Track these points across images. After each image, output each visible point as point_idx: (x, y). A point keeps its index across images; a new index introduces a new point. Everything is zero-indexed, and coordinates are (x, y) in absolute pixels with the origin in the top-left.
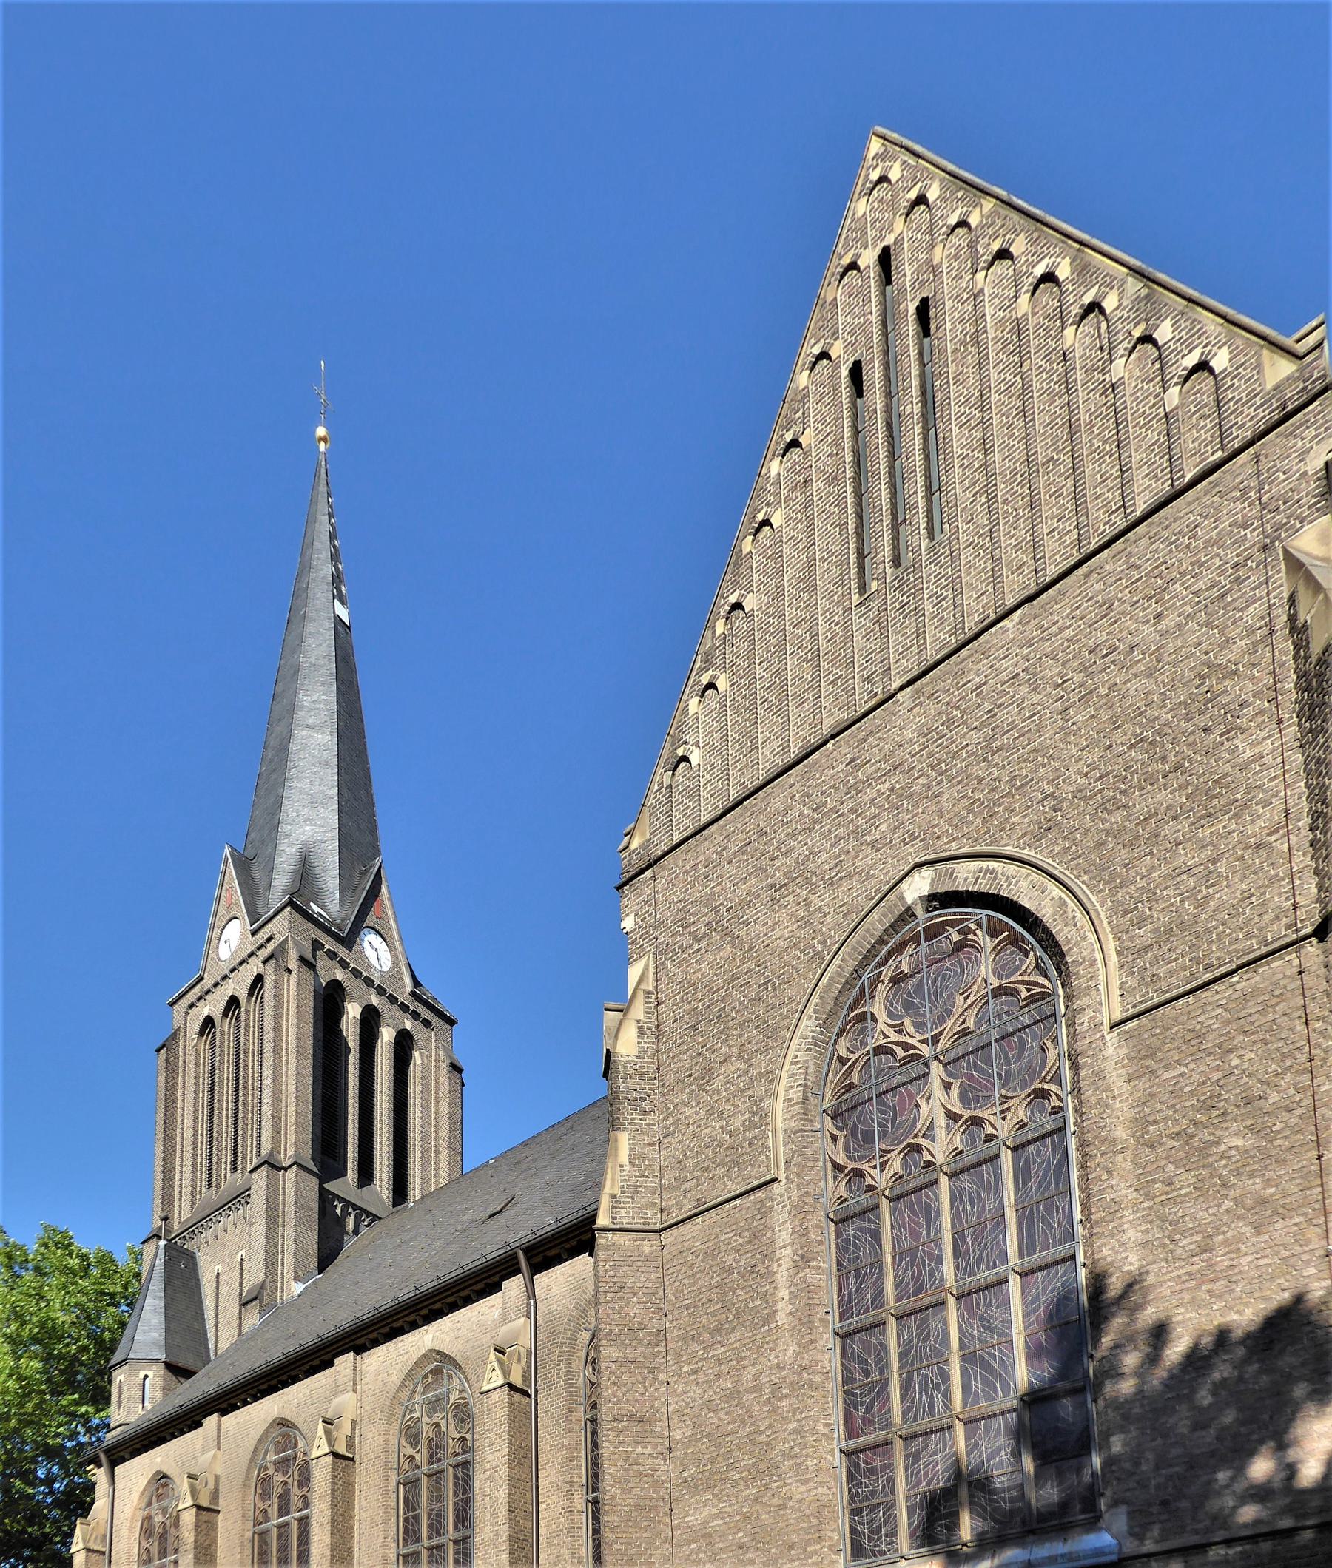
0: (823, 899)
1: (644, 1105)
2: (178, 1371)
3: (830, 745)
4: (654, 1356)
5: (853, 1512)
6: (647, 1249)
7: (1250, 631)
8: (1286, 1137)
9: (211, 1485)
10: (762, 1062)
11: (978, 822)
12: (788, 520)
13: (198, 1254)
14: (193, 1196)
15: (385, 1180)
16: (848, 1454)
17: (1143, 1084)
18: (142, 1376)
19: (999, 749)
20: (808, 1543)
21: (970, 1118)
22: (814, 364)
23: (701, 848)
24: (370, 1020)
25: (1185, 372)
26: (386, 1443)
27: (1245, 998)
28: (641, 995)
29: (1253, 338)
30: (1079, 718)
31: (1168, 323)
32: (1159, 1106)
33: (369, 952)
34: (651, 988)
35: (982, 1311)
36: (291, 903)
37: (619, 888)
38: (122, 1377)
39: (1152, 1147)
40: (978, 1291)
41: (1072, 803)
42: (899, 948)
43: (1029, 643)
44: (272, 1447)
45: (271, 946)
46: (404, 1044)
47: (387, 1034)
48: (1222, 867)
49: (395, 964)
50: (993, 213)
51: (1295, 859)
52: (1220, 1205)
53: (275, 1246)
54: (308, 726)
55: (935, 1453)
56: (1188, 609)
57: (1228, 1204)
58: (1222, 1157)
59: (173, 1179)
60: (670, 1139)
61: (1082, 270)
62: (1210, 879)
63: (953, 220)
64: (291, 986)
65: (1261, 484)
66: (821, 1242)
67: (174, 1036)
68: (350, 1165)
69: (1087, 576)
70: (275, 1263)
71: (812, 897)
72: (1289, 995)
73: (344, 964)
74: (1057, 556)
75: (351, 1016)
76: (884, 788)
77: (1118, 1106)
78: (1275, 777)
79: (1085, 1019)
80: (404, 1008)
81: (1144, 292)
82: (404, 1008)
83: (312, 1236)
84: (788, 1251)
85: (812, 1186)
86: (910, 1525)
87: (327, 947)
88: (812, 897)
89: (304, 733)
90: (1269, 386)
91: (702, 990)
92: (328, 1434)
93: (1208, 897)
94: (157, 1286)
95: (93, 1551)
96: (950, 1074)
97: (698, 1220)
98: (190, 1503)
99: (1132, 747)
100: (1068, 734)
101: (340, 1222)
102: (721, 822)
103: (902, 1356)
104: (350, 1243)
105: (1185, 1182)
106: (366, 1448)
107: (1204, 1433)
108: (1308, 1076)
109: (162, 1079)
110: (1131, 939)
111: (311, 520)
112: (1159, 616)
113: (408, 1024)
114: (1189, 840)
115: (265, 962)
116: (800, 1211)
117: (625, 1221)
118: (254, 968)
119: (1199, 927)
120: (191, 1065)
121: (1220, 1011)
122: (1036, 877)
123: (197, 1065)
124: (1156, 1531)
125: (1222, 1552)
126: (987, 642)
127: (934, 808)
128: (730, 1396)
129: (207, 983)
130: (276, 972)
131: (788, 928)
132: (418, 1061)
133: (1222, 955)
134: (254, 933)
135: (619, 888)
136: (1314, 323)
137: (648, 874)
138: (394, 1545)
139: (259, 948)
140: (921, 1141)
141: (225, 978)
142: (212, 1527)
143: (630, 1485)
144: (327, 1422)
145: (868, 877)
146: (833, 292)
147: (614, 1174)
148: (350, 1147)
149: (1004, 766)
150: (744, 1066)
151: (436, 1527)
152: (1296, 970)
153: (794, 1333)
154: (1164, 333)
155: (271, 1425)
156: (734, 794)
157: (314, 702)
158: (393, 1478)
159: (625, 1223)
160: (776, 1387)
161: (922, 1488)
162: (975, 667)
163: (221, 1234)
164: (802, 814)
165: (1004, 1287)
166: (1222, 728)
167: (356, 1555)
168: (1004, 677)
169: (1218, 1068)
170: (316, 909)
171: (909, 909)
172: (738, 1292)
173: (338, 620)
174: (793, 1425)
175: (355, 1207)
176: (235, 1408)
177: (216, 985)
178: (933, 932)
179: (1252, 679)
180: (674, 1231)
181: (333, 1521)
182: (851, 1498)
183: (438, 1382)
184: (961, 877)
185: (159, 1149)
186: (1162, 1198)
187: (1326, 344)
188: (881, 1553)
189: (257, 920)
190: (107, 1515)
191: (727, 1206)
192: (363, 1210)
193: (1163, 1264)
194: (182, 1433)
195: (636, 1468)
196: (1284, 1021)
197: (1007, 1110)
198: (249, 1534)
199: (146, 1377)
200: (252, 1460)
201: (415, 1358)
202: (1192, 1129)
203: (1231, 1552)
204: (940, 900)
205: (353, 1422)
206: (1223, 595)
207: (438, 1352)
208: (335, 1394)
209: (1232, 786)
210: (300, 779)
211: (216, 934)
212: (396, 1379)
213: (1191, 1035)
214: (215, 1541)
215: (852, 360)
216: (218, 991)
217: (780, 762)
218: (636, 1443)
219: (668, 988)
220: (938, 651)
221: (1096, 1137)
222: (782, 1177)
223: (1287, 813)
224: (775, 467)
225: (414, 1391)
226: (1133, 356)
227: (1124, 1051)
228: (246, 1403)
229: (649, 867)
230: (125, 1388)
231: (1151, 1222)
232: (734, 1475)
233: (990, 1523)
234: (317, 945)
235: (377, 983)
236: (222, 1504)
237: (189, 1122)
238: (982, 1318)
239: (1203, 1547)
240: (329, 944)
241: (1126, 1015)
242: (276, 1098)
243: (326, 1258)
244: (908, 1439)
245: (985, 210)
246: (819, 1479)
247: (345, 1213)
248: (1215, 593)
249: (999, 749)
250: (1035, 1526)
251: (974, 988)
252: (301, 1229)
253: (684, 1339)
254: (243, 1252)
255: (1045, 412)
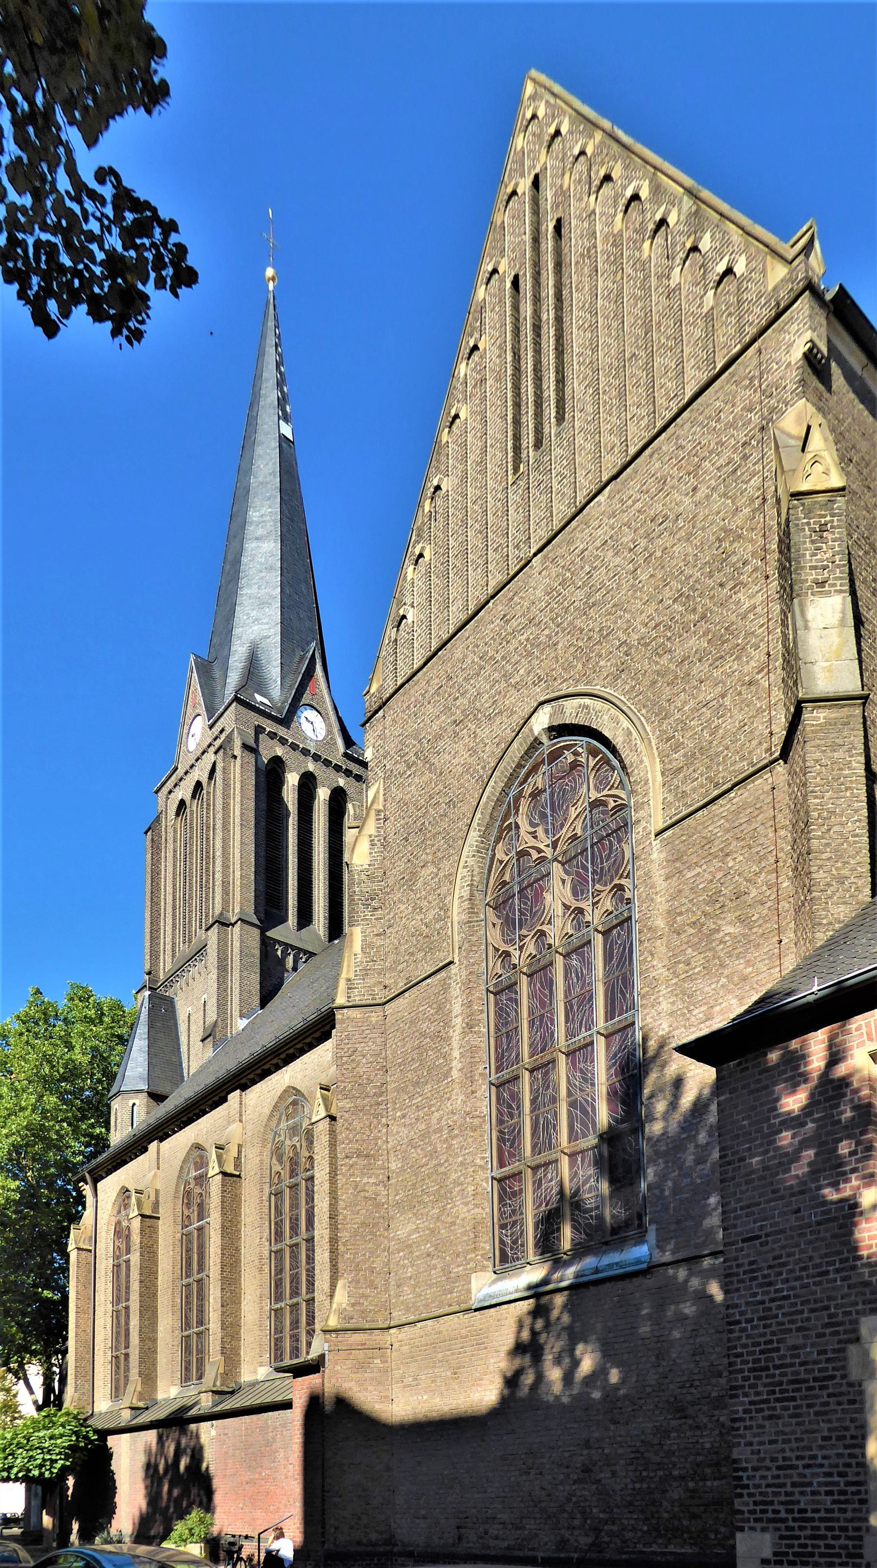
0: (484, 733)
1: (375, 904)
2: (157, 1097)
3: (490, 604)
4: (378, 1104)
5: (503, 1227)
6: (374, 1020)
7: (752, 500)
8: (760, 926)
9: (153, 1198)
10: (446, 865)
11: (580, 666)
12: (473, 413)
13: (176, 999)
14: (173, 951)
15: (322, 920)
16: (500, 1181)
17: (674, 882)
18: (131, 1103)
19: (594, 604)
20: (468, 1252)
21: (576, 908)
22: (489, 280)
23: (412, 692)
24: (308, 783)
25: (718, 278)
26: (261, 1162)
27: (738, 812)
28: (373, 814)
29: (761, 246)
30: (643, 577)
31: (708, 235)
32: (683, 900)
33: (306, 727)
34: (381, 808)
35: (582, 1065)
36: (236, 699)
37: (363, 725)
38: (116, 1106)
39: (679, 934)
40: (580, 1049)
41: (637, 648)
42: (534, 769)
43: (613, 515)
44: (192, 1167)
45: (223, 736)
46: (338, 799)
47: (323, 794)
48: (727, 701)
49: (329, 732)
50: (602, 143)
51: (773, 694)
52: (718, 982)
53: (225, 990)
54: (257, 539)
55: (551, 1180)
56: (713, 483)
57: (724, 980)
58: (721, 942)
59: (158, 938)
60: (391, 929)
61: (657, 189)
62: (720, 711)
63: (576, 151)
64: (236, 768)
65: (761, 373)
66: (482, 1011)
67: (158, 819)
68: (290, 912)
69: (651, 456)
70: (225, 1005)
71: (478, 730)
72: (765, 807)
73: (283, 741)
74: (637, 436)
75: (290, 784)
76: (523, 638)
77: (659, 900)
78: (763, 625)
79: (640, 829)
80: (338, 768)
81: (694, 208)
82: (338, 768)
83: (255, 978)
84: (459, 1020)
85: (476, 967)
86: (535, 1237)
87: (268, 729)
88: (478, 730)
89: (254, 545)
90: (770, 288)
91: (412, 808)
92: (219, 1157)
93: (718, 727)
94: (142, 1030)
95: (82, 1250)
96: (567, 872)
97: (407, 994)
98: (136, 1213)
99: (675, 601)
100: (635, 591)
101: (281, 962)
102: (425, 669)
103: (533, 1101)
104: (290, 979)
105: (698, 960)
106: (249, 1166)
107: (703, 1166)
108: (774, 875)
109: (149, 856)
110: (670, 762)
111: (261, 353)
112: (695, 489)
113: (341, 782)
114: (708, 679)
115: (216, 753)
116: (468, 987)
117: (357, 998)
118: (210, 757)
119: (712, 752)
120: (170, 841)
121: (722, 821)
122: (614, 711)
123: (175, 841)
124: (670, 1246)
125: (712, 1262)
126: (588, 514)
127: (552, 655)
128: (424, 1135)
129: (180, 772)
130: (224, 761)
131: (464, 757)
132: (352, 812)
133: (726, 775)
134: (211, 727)
135: (363, 725)
136: (805, 228)
137: (381, 713)
138: (267, 1244)
139: (215, 739)
140: (545, 928)
141: (192, 766)
142: (154, 1230)
143: (358, 1208)
144: (219, 1147)
145: (513, 713)
146: (502, 217)
147: (349, 962)
148: (290, 896)
149: (597, 619)
150: (435, 870)
151: (295, 1229)
152: (769, 787)
153: (462, 1085)
154: (705, 244)
155: (190, 1149)
156: (434, 645)
157: (262, 516)
158: (267, 1190)
159: (357, 1000)
160: (451, 1128)
161: (543, 1208)
162: (580, 536)
163: (191, 981)
164: (473, 662)
165: (589, 1048)
166: (731, 584)
167: (243, 1251)
168: (598, 543)
169: (720, 869)
170: (259, 698)
171: (536, 739)
172: (430, 1053)
173: (283, 438)
174: (460, 1159)
175: (293, 948)
176: (168, 1136)
177: (186, 773)
178: (555, 756)
179: (751, 541)
180: (392, 1004)
181: (223, 1227)
182: (502, 1214)
183: (295, 1111)
184: (568, 712)
185: (148, 915)
186: (683, 976)
187: (817, 244)
188: (518, 1259)
189: (213, 714)
190: (92, 1222)
191: (424, 983)
192: (300, 950)
193: (683, 1030)
194: (137, 1156)
195: (362, 1194)
196: (761, 830)
197: (598, 902)
198: (179, 1235)
199: (134, 1104)
200: (179, 1177)
201: (279, 1094)
202: (703, 920)
203: (717, 1262)
204: (559, 730)
205: (240, 1146)
206: (735, 470)
207: (294, 1088)
208: (229, 1124)
209: (736, 632)
210: (249, 586)
211: (185, 731)
212: (267, 1111)
213: (705, 841)
214: (156, 1242)
215: (513, 274)
216: (188, 778)
217: (463, 617)
218: (363, 1174)
219: (392, 806)
220: (560, 521)
221: (645, 926)
222: (456, 960)
223: (769, 654)
224: (462, 369)
225: (280, 1119)
226: (687, 263)
227: (664, 855)
228: (175, 1132)
229: (380, 708)
230: (119, 1114)
231: (676, 995)
232: (426, 1199)
233: (583, 1236)
234: (259, 730)
235: (313, 751)
236: (162, 1212)
237: (169, 889)
238: (581, 1070)
239: (700, 1257)
240: (269, 726)
241: (666, 824)
242: (225, 866)
243: (267, 996)
244: (535, 1169)
245: (597, 141)
246: (476, 1202)
247: (285, 954)
248: (730, 468)
249: (594, 604)
250: (608, 1238)
251: (580, 803)
252: (245, 974)
253: (398, 1090)
254: (205, 996)
255: (632, 312)
